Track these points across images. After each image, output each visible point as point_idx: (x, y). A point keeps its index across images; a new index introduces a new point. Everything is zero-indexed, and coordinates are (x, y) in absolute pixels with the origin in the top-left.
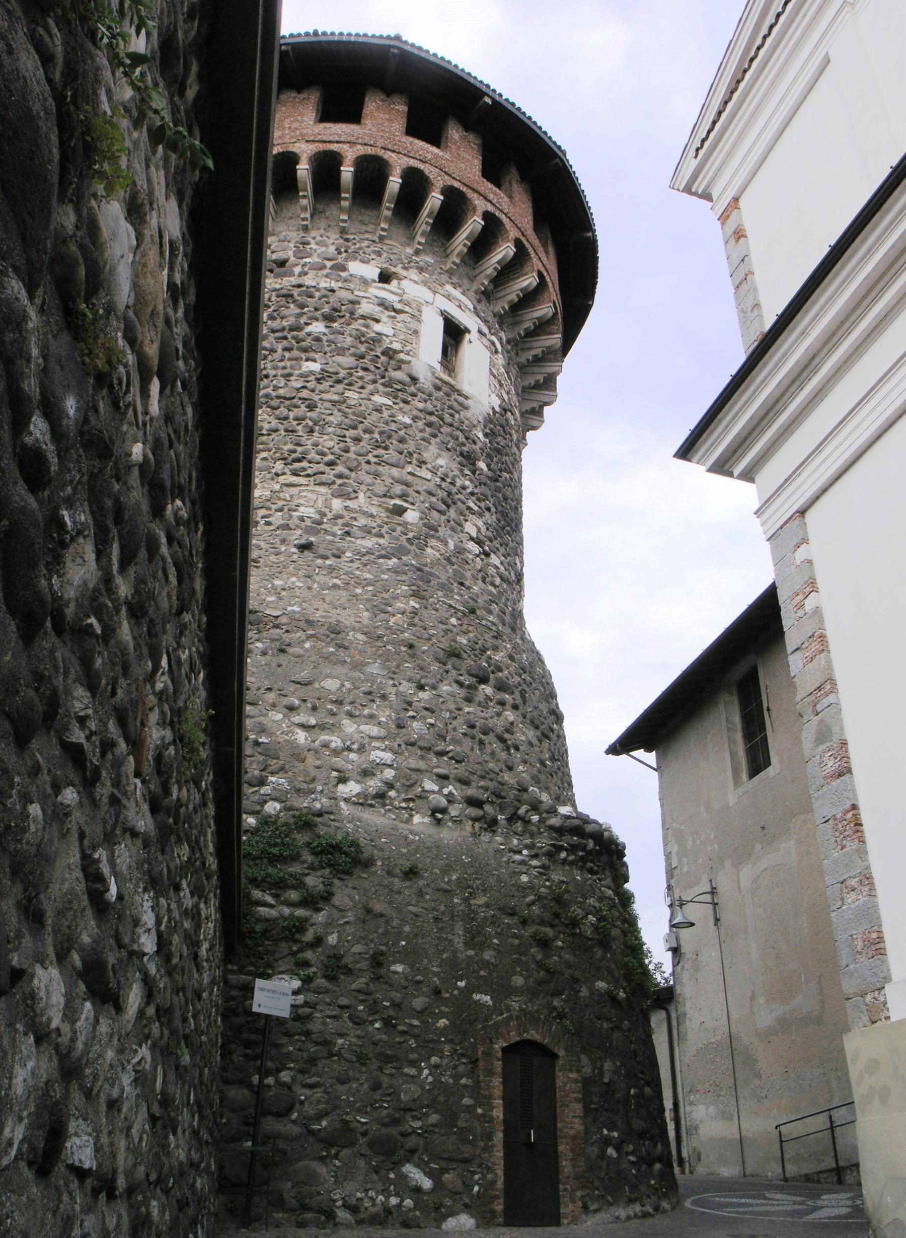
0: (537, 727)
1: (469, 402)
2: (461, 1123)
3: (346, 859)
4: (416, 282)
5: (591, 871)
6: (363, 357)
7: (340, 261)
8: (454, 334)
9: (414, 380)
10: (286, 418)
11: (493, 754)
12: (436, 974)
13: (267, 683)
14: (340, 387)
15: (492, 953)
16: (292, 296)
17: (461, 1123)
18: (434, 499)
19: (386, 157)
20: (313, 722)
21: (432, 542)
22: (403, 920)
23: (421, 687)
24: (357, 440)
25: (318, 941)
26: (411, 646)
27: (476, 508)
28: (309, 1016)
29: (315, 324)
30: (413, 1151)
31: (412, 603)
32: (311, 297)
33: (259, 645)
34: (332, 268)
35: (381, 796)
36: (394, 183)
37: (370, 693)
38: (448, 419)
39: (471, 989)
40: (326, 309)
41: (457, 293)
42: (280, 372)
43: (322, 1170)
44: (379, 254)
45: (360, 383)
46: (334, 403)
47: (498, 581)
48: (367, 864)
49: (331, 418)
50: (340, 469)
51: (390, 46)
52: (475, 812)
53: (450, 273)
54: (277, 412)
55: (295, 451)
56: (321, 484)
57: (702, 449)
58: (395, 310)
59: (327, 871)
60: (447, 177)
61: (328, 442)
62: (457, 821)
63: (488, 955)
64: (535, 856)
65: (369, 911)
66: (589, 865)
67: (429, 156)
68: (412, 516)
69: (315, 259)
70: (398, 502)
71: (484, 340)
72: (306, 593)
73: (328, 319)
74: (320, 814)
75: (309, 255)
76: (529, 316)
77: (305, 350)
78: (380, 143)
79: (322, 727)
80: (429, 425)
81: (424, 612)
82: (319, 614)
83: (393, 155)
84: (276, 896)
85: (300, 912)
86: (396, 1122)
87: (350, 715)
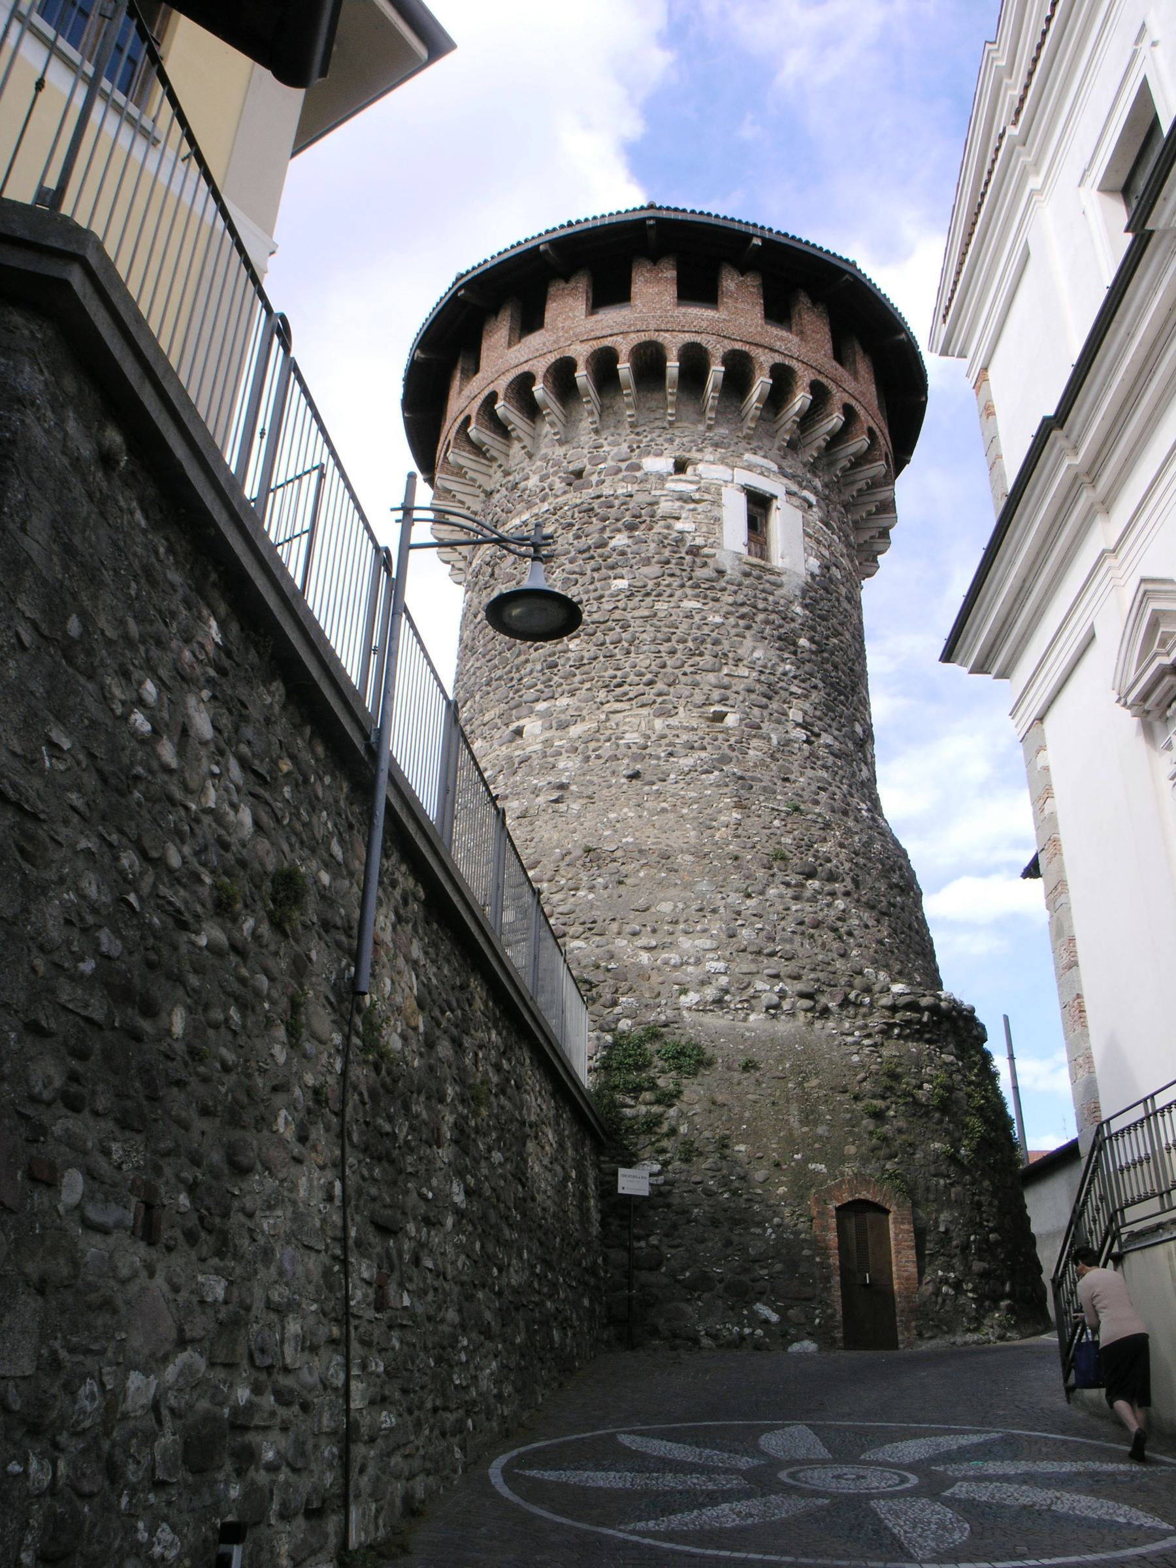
0: (873, 908)
1: (784, 578)
2: (802, 1270)
3: (691, 1059)
4: (713, 463)
5: (929, 1042)
6: (668, 562)
7: (634, 460)
8: (759, 504)
9: (721, 573)
10: (603, 644)
11: (824, 945)
12: (774, 1150)
13: (611, 915)
14: (649, 600)
15: (825, 1127)
16: (592, 509)
17: (802, 1270)
18: (753, 696)
19: (660, 340)
20: (654, 943)
21: (755, 743)
22: (743, 1107)
23: (749, 896)
24: (673, 652)
25: (673, 1132)
26: (736, 858)
27: (799, 691)
28: (670, 1192)
29: (618, 536)
30: (762, 1293)
31: (735, 815)
32: (611, 507)
33: (600, 880)
34: (627, 469)
35: (719, 1002)
36: (673, 366)
37: (701, 910)
38: (761, 605)
39: (806, 1160)
40: (627, 518)
41: (757, 459)
42: (592, 595)
43: (689, 1309)
44: (671, 441)
45: (669, 591)
46: (645, 618)
47: (830, 760)
48: (710, 1063)
49: (644, 636)
50: (660, 686)
51: (644, 220)
52: (807, 1003)
53: (748, 438)
54: (594, 639)
55: (615, 677)
56: (643, 706)
57: (962, 648)
58: (694, 501)
59: (674, 1073)
60: (726, 341)
61: (643, 661)
62: (792, 1014)
63: (821, 1130)
64: (869, 1036)
65: (714, 1103)
66: (927, 1036)
67: (704, 324)
68: (731, 720)
69: (610, 463)
70: (718, 708)
71: (795, 501)
72: (638, 822)
73: (631, 528)
74: (666, 1025)
75: (605, 460)
76: (843, 454)
77: (612, 568)
78: (652, 327)
79: (664, 947)
80: (742, 617)
81: (747, 821)
82: (650, 841)
83: (667, 335)
84: (636, 1098)
85: (655, 1109)
86: (746, 1271)
87: (686, 933)
